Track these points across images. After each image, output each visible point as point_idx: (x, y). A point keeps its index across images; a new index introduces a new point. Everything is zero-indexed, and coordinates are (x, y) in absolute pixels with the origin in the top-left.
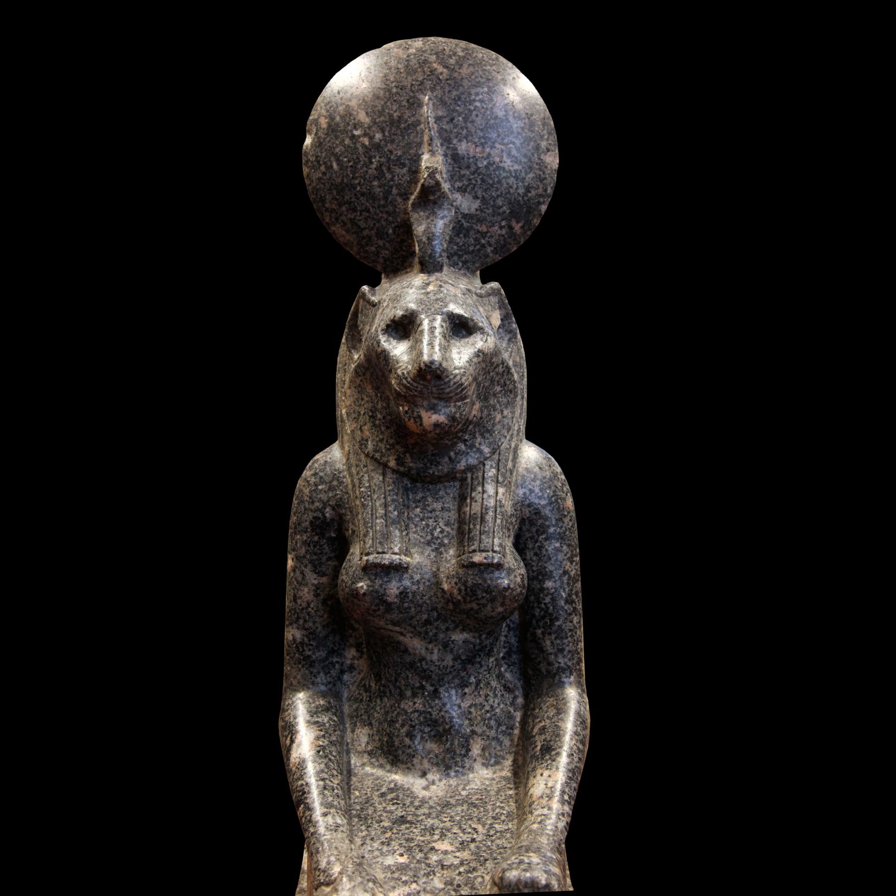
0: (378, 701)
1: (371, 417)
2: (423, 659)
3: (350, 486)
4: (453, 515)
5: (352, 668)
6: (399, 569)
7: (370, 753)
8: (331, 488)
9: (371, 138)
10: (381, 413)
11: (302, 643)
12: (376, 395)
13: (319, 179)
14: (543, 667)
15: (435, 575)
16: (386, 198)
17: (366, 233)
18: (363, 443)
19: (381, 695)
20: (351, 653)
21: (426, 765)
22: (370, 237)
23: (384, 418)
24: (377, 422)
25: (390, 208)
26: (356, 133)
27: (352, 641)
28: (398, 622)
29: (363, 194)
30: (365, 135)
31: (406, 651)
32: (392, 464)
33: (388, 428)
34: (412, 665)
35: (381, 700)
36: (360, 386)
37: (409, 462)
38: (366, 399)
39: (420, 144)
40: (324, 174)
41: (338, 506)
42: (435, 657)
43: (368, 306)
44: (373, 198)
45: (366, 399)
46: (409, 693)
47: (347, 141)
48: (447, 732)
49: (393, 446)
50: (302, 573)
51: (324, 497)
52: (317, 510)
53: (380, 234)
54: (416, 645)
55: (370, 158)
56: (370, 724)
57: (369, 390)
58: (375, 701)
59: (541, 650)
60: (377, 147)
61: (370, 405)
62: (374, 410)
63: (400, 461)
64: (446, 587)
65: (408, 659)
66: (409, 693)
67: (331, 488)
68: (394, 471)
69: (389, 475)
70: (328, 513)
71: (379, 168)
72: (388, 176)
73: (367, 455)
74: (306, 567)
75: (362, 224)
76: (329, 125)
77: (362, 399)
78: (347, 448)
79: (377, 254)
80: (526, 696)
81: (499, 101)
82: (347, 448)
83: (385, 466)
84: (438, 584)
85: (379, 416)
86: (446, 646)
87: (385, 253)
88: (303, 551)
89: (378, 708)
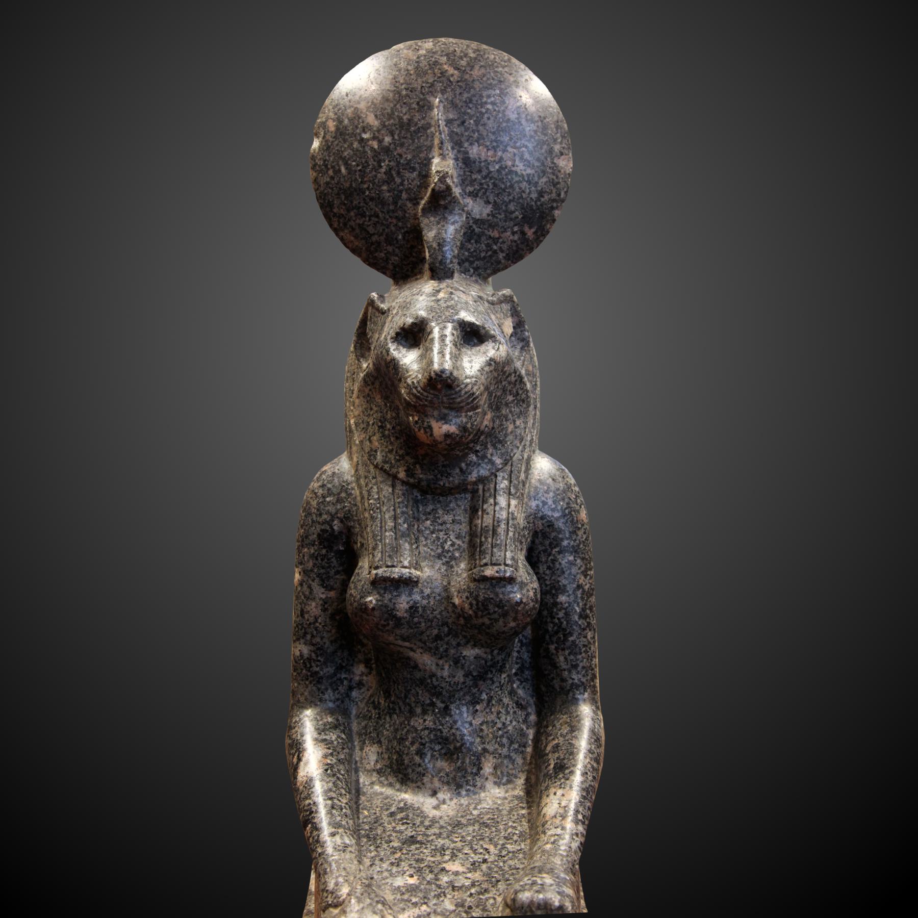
0: (388, 718)
1: (380, 427)
2: (433, 675)
3: (359, 498)
4: (464, 528)
5: (360, 684)
6: (409, 583)
7: (379, 772)
8: (340, 500)
9: (380, 142)
10: (390, 423)
11: (309, 659)
12: (386, 405)
13: (327, 183)
14: (556, 683)
15: (446, 589)
16: (395, 203)
17: (375, 238)
18: (372, 454)
19: (391, 712)
20: (360, 669)
21: (437, 784)
22: (379, 243)
23: (393, 428)
24: (387, 432)
25: (400, 213)
26: (365, 136)
27: (360, 656)
28: (408, 637)
29: (372, 199)
30: (374, 138)
31: (416, 667)
32: (402, 475)
33: (397, 438)
34: (422, 682)
35: (390, 717)
36: (368, 395)
37: (419, 473)
38: (375, 409)
39: (430, 148)
40: (332, 178)
41: (347, 518)
42: (446, 673)
43: (377, 314)
44: (382, 203)
45: (375, 409)
46: (419, 710)
47: (356, 145)
48: (458, 750)
49: (402, 457)
50: (310, 587)
51: (332, 509)
52: (325, 522)
53: (390, 240)
54: (426, 661)
55: (379, 162)
56: (379, 742)
57: (378, 399)
58: (385, 719)
59: (555, 666)
60: (387, 150)
61: (380, 414)
62: (383, 420)
63: (410, 472)
64: (457, 601)
65: (418, 675)
66: (419, 710)
67: (340, 500)
68: (404, 483)
69: (399, 487)
70: (337, 525)
71: (388, 172)
72: (398, 180)
73: (376, 467)
74: (313, 581)
75: (371, 230)
76: (337, 128)
77: (371, 409)
78: (355, 459)
79: (387, 260)
80: (539, 713)
81: (511, 104)
82: (355, 459)
83: (395, 477)
84: (449, 598)
85: (388, 426)
86: (457, 662)
87: (395, 259)
88: (311, 564)
89: (387, 726)
